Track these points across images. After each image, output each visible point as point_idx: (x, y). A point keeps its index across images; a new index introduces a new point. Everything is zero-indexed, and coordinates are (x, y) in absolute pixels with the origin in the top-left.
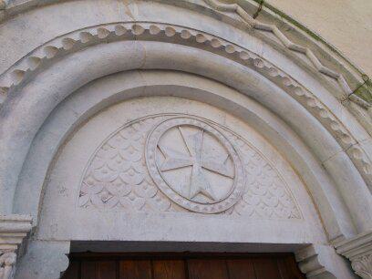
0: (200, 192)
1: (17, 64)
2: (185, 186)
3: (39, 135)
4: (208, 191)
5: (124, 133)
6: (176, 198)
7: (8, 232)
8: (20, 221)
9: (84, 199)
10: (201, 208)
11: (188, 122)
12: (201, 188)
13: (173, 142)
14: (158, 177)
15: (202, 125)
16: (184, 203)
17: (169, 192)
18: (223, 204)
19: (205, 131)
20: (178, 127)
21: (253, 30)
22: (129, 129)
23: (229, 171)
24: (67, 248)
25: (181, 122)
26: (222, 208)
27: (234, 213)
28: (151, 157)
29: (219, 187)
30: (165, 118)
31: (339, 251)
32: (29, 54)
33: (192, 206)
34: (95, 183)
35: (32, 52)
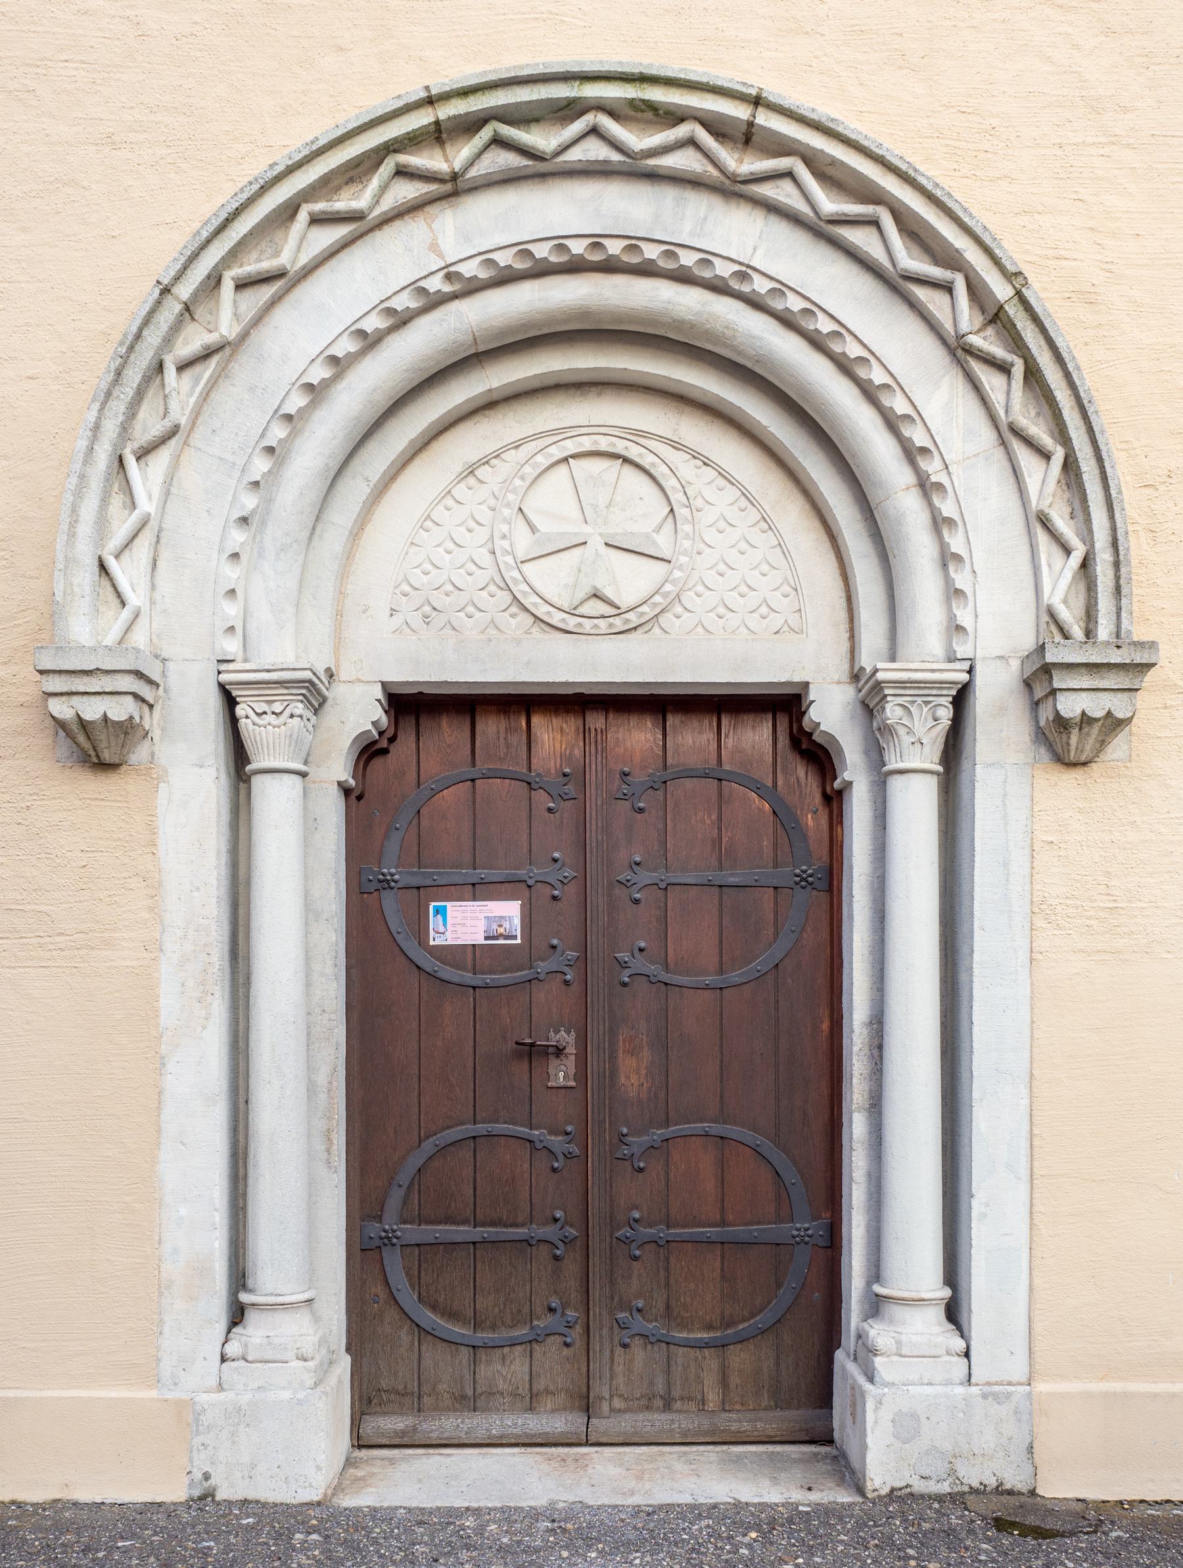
0: (595, 595)
1: (262, 436)
2: (566, 585)
3: (318, 530)
4: (609, 592)
5: (460, 491)
6: (542, 610)
7: (941, 683)
8: (1112, 517)
9: (398, 619)
10: (588, 624)
11: (587, 444)
12: (595, 588)
13: (554, 502)
14: (516, 574)
15: (620, 447)
16: (557, 618)
17: (530, 600)
18: (631, 616)
19: (626, 460)
20: (565, 460)
21: (732, 189)
22: (471, 480)
23: (663, 543)
24: (378, 693)
25: (571, 447)
26: (627, 622)
27: (656, 630)
28: (504, 537)
29: (631, 581)
30: (541, 443)
31: (224, 678)
32: (276, 411)
33: (572, 623)
34: (412, 592)
35: (279, 407)
